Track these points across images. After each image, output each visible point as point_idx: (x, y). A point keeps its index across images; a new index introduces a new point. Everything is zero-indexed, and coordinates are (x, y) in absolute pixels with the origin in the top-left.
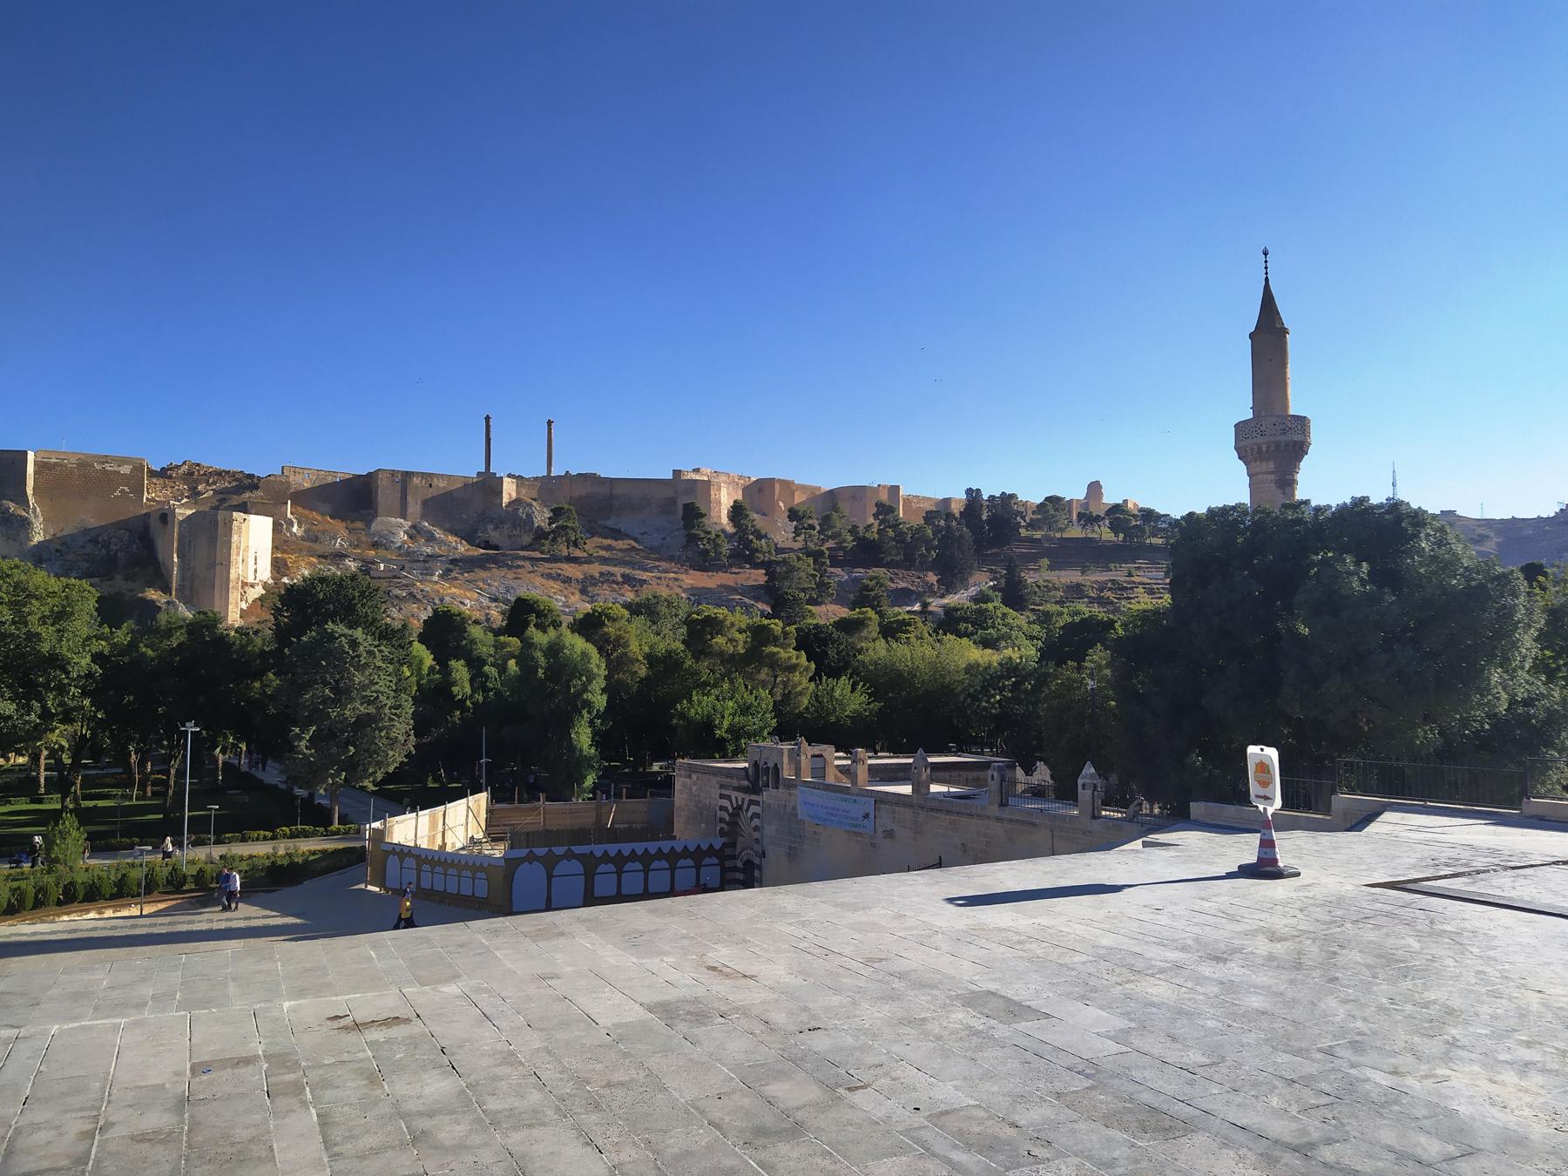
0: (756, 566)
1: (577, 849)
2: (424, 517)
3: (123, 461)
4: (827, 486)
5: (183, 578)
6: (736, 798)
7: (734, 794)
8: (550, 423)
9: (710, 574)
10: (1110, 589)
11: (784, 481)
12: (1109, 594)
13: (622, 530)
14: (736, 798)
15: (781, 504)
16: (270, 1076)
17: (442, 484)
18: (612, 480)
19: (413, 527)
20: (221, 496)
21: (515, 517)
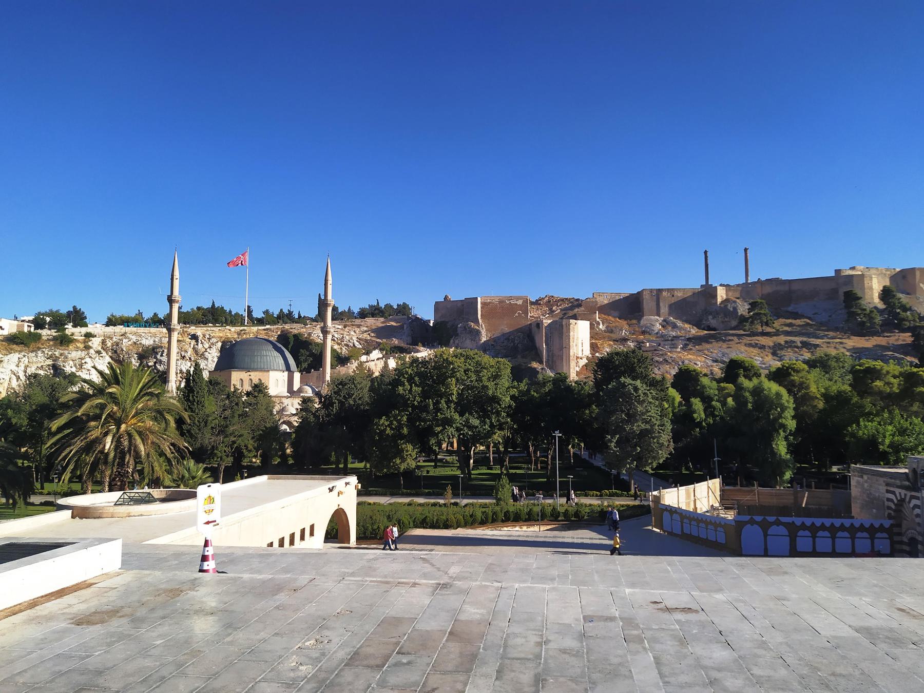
0: (904, 331)
2: (670, 314)
3: (518, 298)
5: (548, 356)
6: (900, 493)
7: (897, 491)
8: (746, 250)
9: (867, 338)
14: (900, 493)
17: (680, 294)
19: (664, 321)
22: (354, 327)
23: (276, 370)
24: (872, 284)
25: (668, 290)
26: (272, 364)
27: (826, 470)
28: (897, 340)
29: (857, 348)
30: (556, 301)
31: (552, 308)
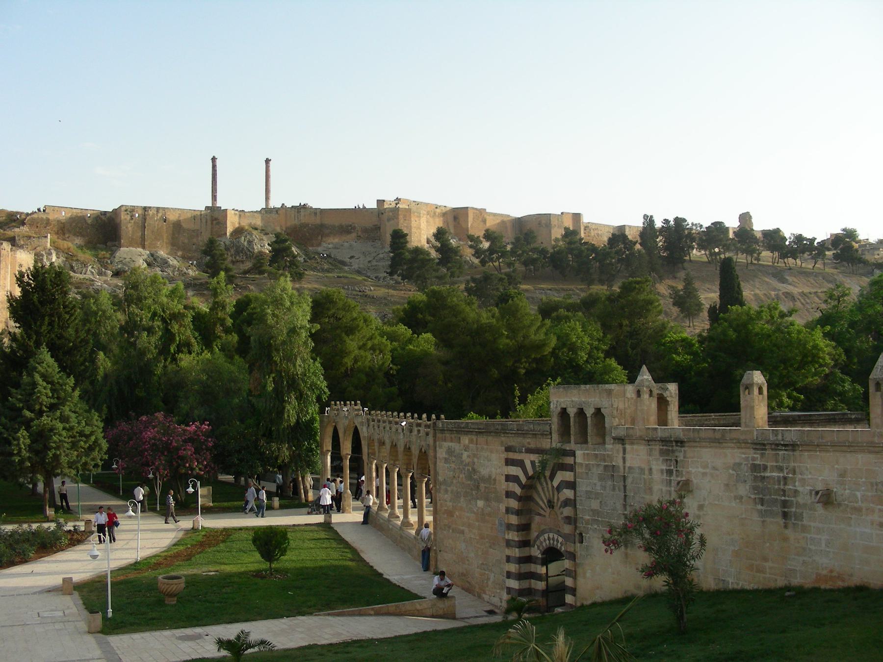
6: (533, 463)
18: (323, 211)
24: (420, 223)
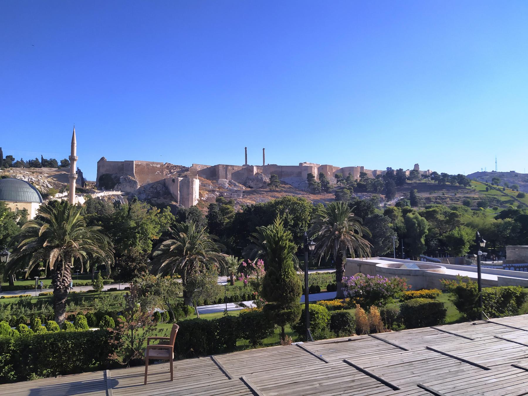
0: (330, 193)
1: (513, 265)
2: (232, 179)
3: (157, 164)
4: (341, 167)
5: (181, 198)
8: (264, 149)
9: (316, 195)
10: (439, 199)
11: (330, 165)
12: (439, 200)
13: (286, 182)
15: (329, 173)
16: (140, 375)
17: (236, 169)
19: (230, 182)
20: (179, 173)
21: (258, 179)
22: (37, 173)
23: (35, 202)
25: (231, 166)
26: (32, 198)
27: (24, 270)
28: (328, 197)
29: (315, 200)
30: (171, 167)
31: (171, 171)
